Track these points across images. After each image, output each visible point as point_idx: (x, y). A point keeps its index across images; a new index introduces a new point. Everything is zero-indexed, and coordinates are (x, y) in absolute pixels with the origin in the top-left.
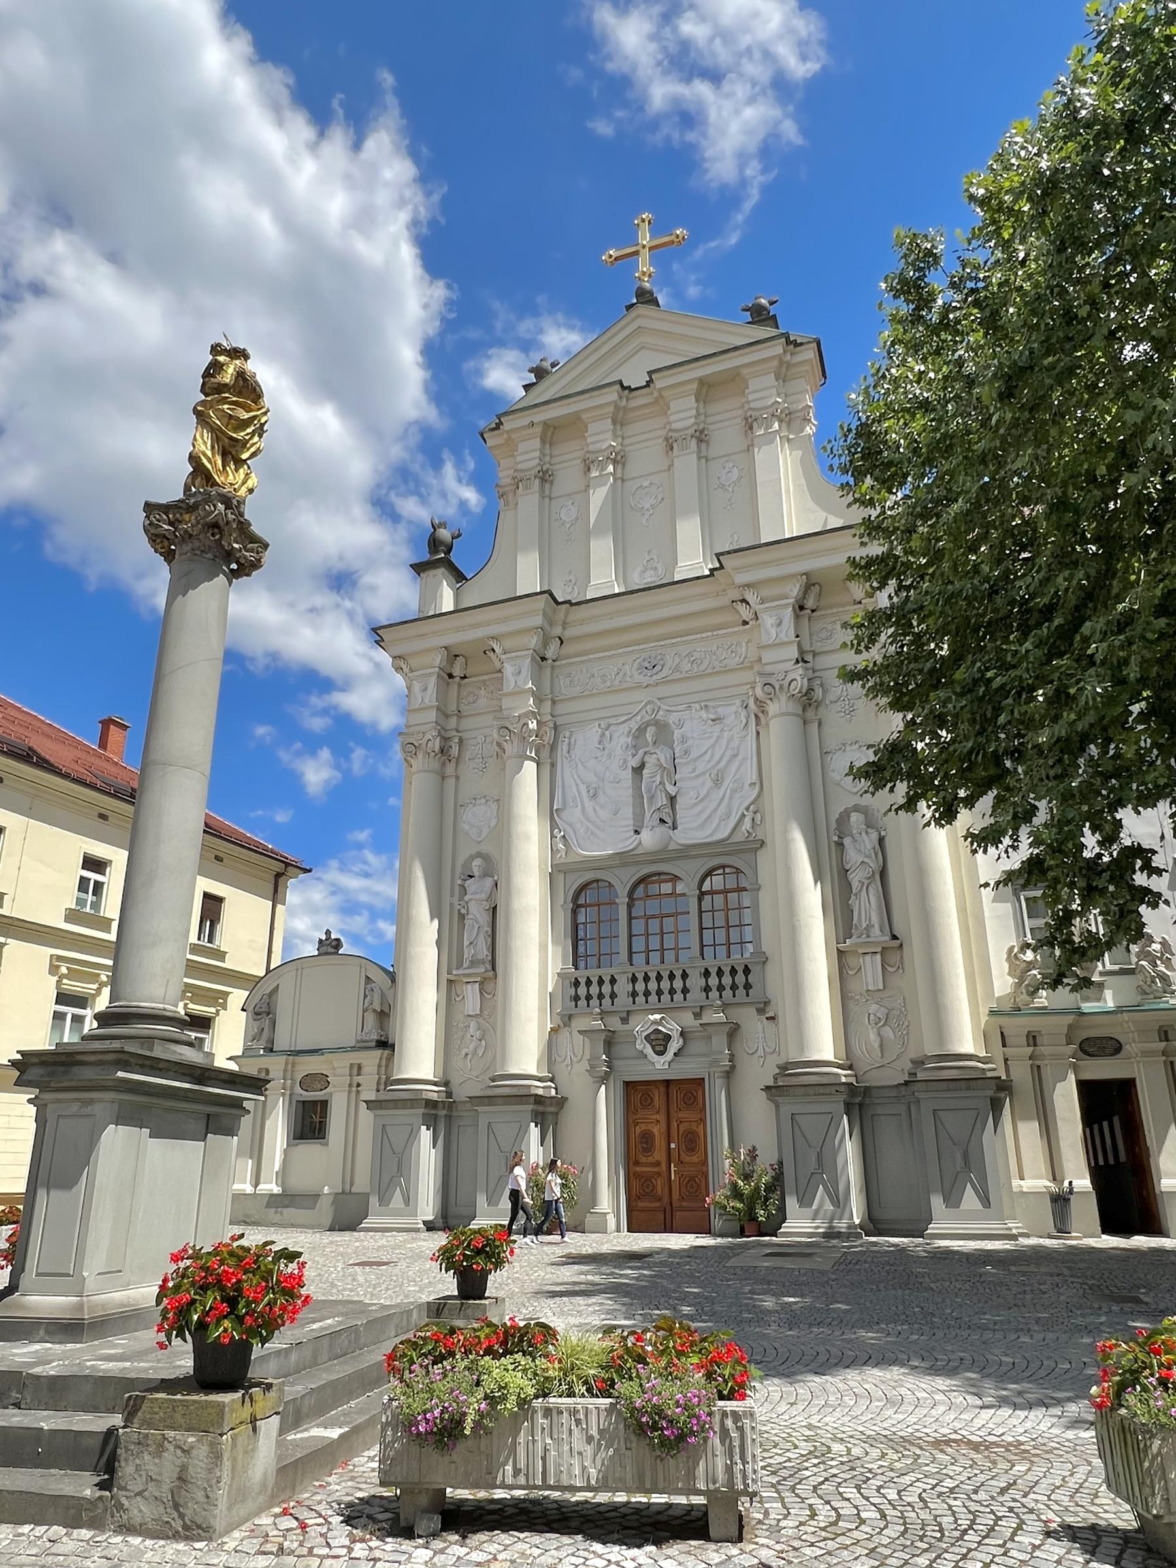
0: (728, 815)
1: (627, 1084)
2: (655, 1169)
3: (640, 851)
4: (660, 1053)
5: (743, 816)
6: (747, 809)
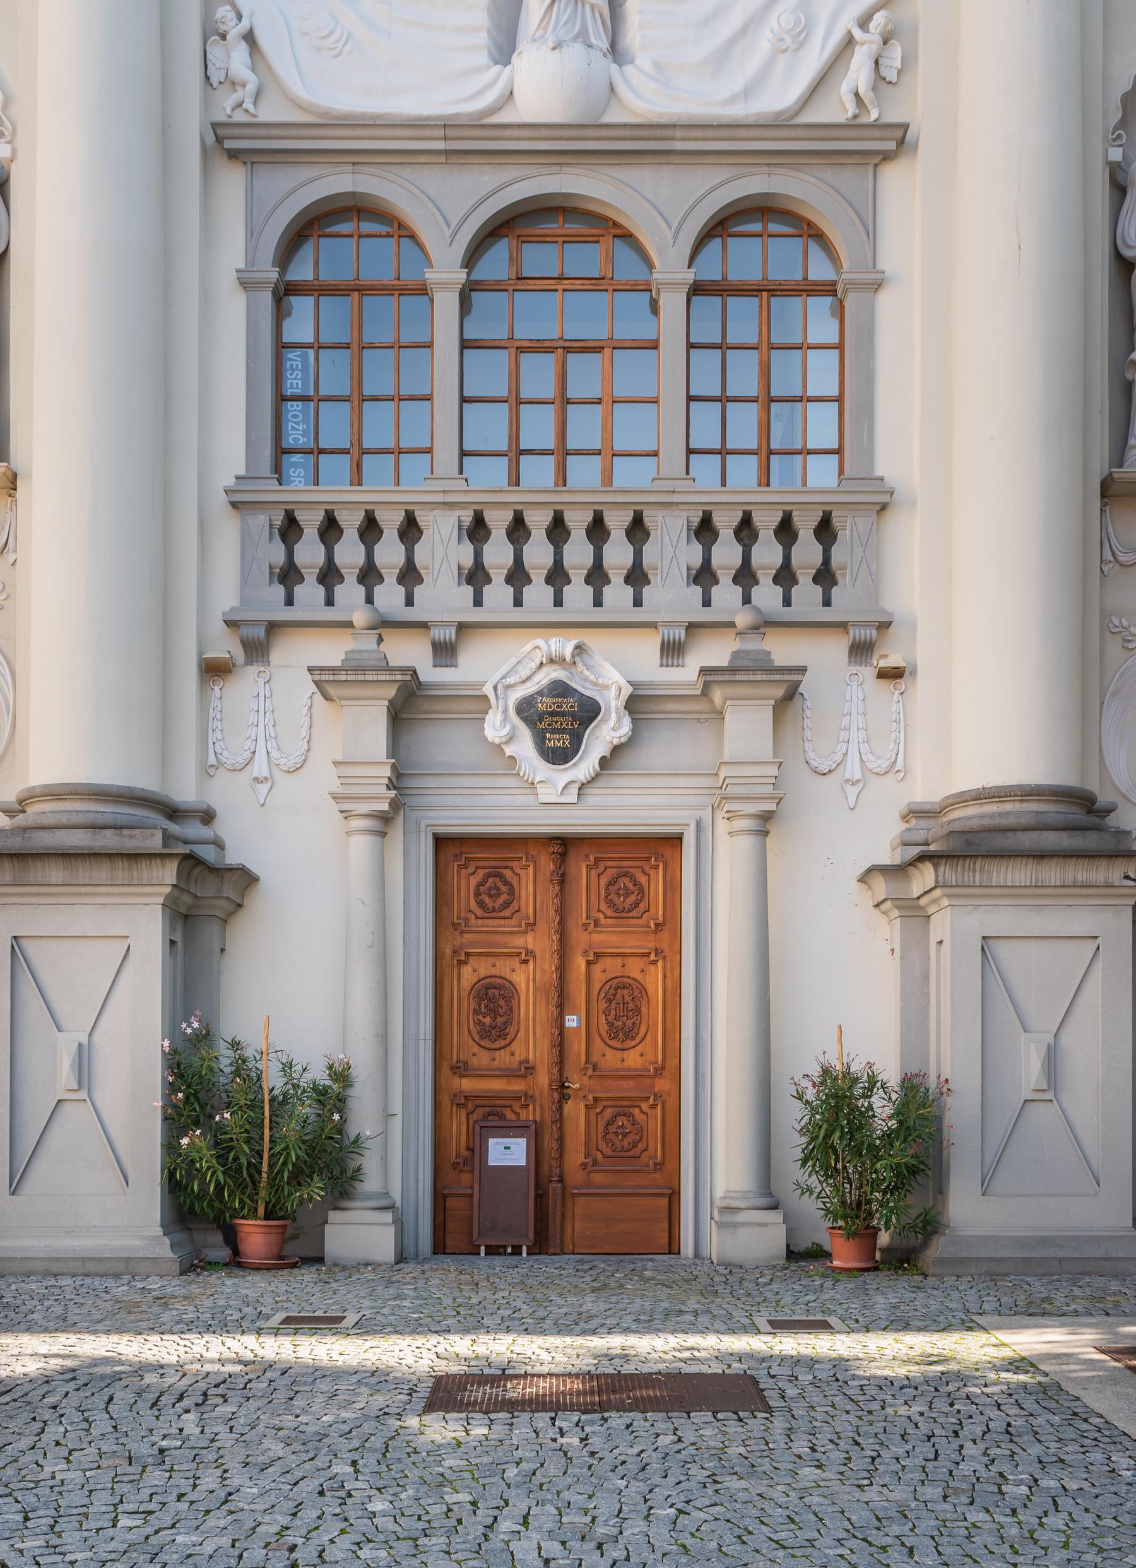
0: (801, 37)
1: (440, 841)
2: (518, 1086)
3: (504, 117)
4: (559, 757)
5: (849, 42)
6: (864, 23)
